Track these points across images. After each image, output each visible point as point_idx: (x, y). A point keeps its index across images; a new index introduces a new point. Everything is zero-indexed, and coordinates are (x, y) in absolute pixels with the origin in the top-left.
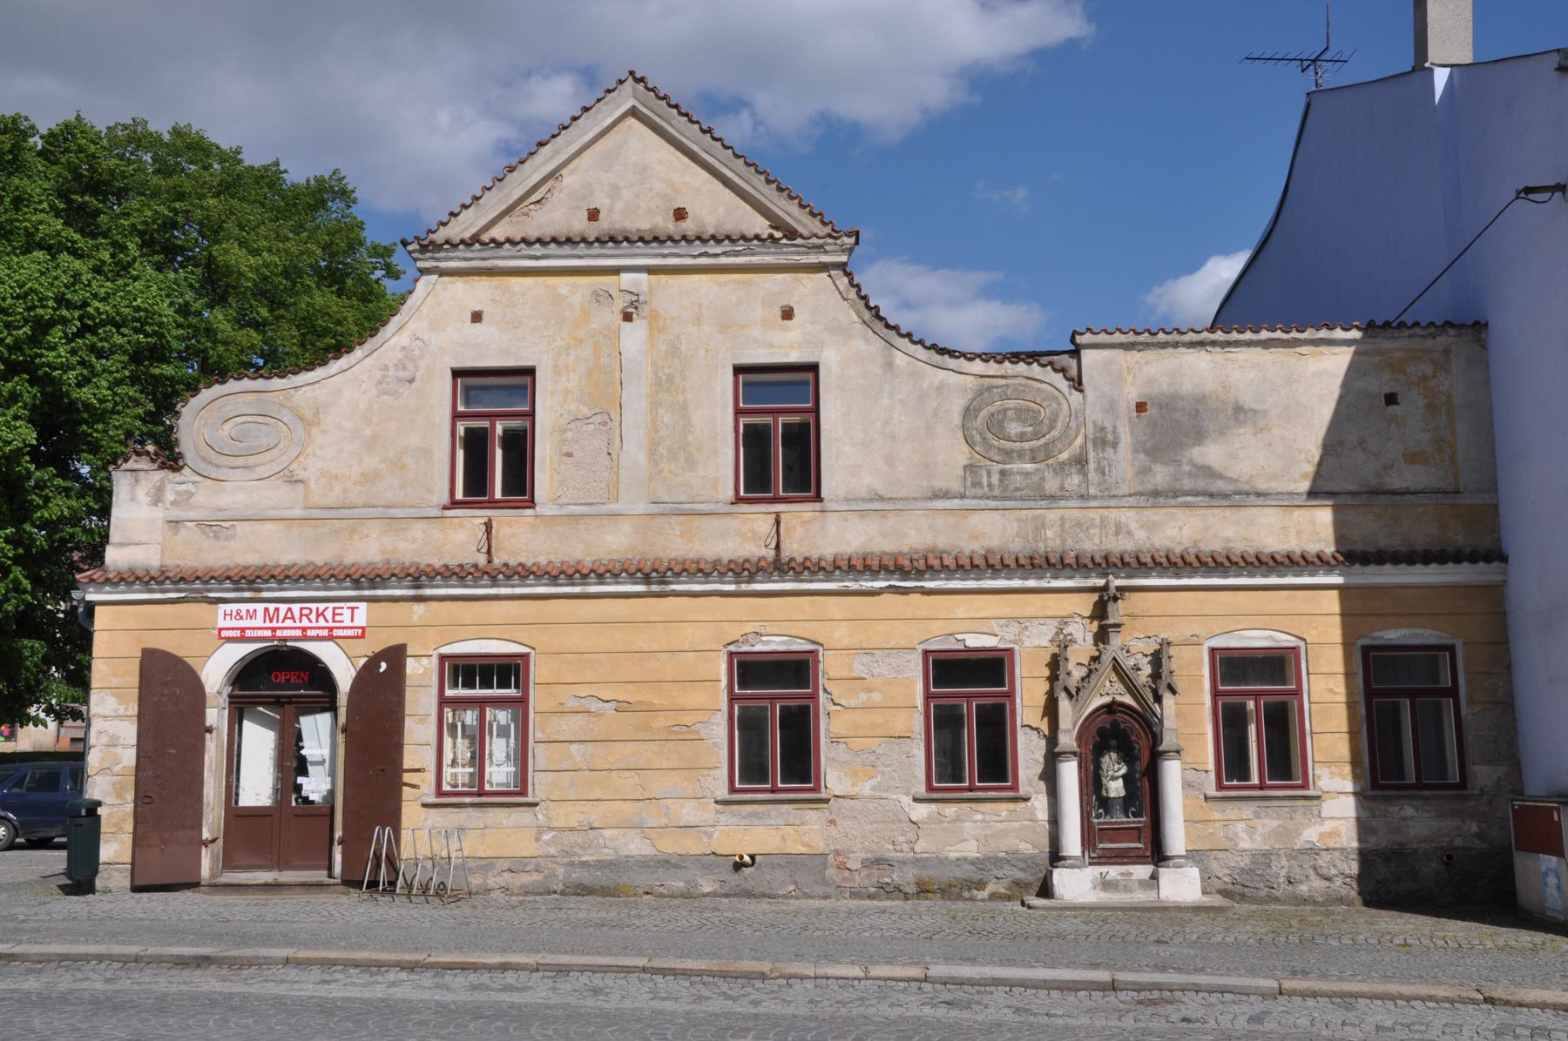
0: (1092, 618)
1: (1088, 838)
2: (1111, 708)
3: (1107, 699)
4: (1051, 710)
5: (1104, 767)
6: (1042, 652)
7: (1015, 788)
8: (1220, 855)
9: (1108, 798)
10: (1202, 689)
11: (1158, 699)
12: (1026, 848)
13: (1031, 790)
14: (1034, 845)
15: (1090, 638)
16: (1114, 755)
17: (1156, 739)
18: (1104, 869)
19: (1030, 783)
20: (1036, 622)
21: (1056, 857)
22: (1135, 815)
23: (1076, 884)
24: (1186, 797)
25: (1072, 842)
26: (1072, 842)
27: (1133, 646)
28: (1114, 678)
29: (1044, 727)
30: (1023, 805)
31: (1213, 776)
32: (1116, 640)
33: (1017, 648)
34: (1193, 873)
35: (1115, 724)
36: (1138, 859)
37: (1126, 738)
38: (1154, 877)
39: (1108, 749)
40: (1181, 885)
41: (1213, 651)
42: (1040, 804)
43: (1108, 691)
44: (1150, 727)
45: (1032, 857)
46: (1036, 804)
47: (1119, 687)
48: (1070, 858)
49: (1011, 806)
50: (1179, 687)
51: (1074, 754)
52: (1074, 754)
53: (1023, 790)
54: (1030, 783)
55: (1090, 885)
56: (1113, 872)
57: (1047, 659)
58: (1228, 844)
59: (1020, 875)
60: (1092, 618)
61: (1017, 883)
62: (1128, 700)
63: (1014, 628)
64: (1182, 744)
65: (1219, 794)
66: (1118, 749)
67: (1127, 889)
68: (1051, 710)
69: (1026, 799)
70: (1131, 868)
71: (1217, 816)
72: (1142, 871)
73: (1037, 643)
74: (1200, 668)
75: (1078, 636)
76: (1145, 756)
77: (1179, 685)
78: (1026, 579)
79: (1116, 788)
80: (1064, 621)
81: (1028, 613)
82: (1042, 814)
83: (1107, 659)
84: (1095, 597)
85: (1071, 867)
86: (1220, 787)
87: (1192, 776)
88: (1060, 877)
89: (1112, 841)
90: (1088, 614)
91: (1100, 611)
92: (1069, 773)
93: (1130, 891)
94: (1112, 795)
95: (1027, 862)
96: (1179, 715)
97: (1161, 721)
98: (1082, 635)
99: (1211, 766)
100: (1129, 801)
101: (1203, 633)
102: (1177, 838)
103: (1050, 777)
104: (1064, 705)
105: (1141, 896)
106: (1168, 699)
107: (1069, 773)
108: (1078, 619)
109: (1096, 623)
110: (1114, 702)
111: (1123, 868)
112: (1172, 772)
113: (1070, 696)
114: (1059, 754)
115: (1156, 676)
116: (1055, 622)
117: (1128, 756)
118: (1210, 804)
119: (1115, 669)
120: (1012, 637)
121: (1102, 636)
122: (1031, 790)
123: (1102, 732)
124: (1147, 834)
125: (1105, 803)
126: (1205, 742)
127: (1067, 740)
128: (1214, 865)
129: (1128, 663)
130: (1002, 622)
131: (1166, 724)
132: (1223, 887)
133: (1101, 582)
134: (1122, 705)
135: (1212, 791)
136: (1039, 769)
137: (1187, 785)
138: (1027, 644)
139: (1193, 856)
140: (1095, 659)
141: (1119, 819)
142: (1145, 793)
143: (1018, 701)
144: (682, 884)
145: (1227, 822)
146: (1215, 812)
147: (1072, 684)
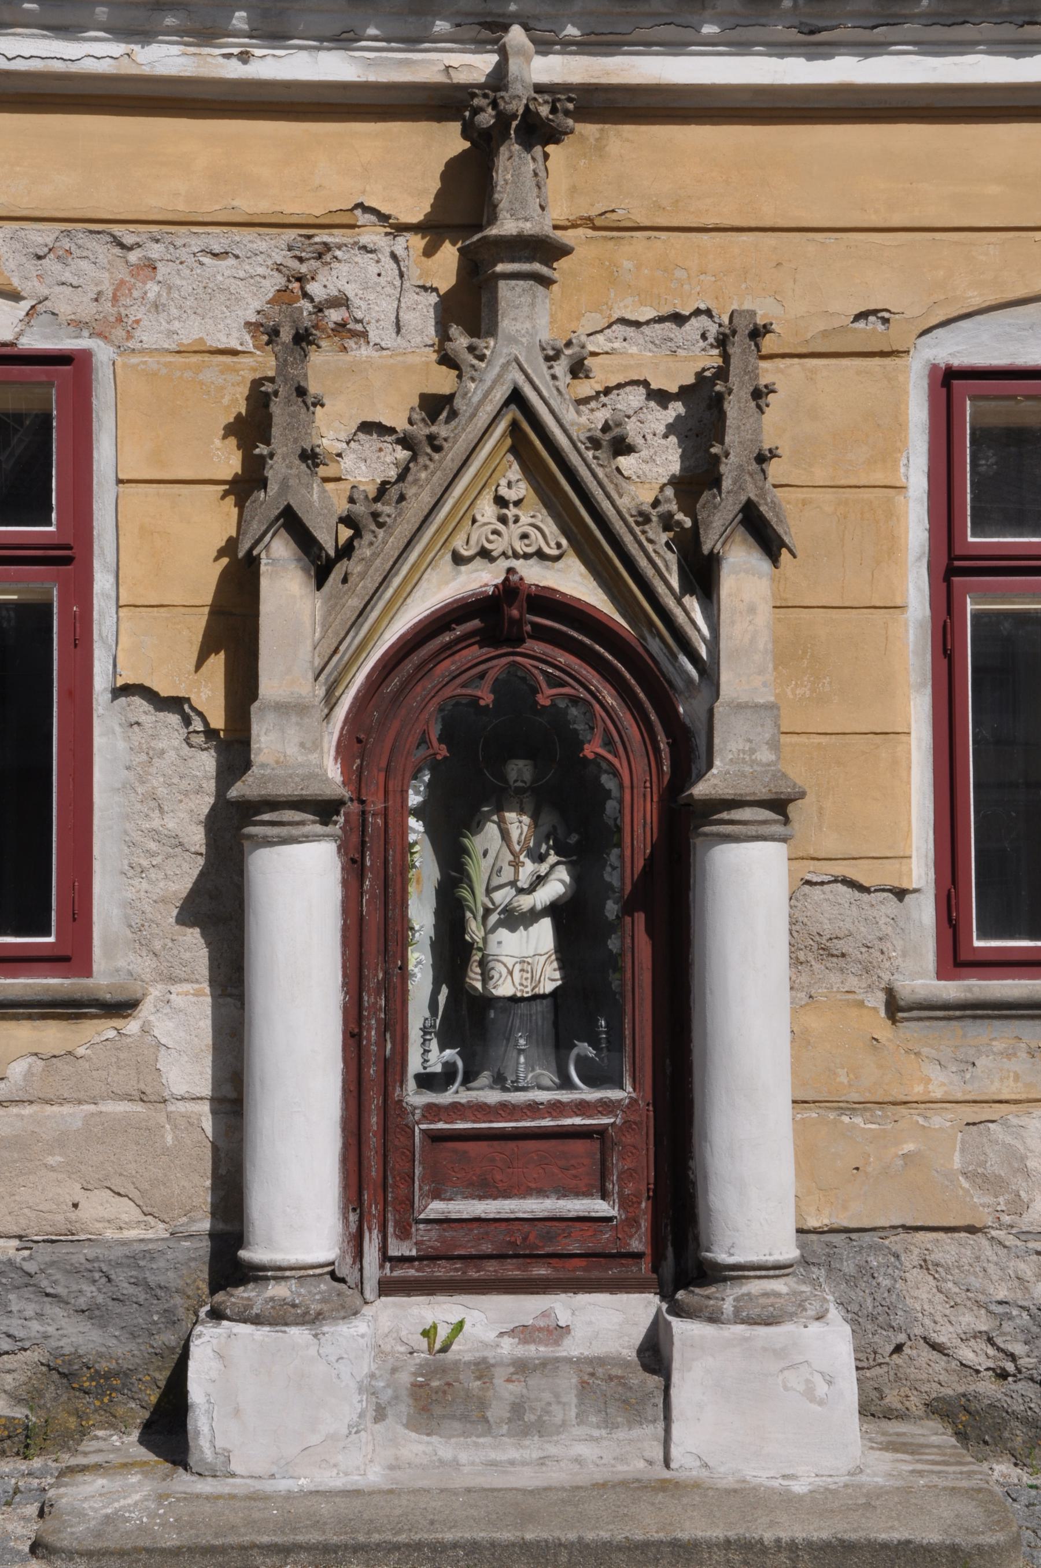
0: (433, 230)
1: (379, 1163)
2: (499, 616)
3: (482, 578)
4: (233, 626)
5: (479, 870)
6: (213, 370)
7: (73, 957)
8: (947, 1249)
9: (488, 1001)
10: (891, 546)
11: (702, 575)
12: (114, 1220)
13: (143, 965)
14: (139, 1211)
15: (421, 316)
16: (519, 824)
17: (686, 749)
18: (441, 1311)
19: (140, 936)
20: (196, 240)
21: (229, 1264)
22: (592, 1080)
23: (292, 1407)
24: (804, 999)
25: (301, 1209)
26: (301, 1209)
27: (610, 341)
28: (515, 483)
29: (209, 695)
30: (105, 1029)
31: (924, 911)
32: (528, 317)
33: (103, 353)
34: (829, 1344)
35: (516, 690)
36: (591, 1265)
37: (557, 740)
38: (655, 1354)
39: (501, 798)
40: (773, 1410)
41: (948, 380)
42: (178, 1025)
43: (496, 540)
44: (665, 693)
45: (137, 1258)
46: (164, 1029)
47: (538, 525)
48: (279, 1272)
49: (52, 1035)
50: (795, 523)
51: (324, 810)
52: (324, 810)
53: (109, 967)
54: (140, 936)
55: (351, 1406)
56: (483, 1323)
57: (235, 402)
58: (980, 1205)
59: (78, 1337)
60: (433, 230)
61: (66, 1372)
62: (574, 581)
63: (96, 266)
64: (798, 774)
65: (953, 990)
66: (539, 801)
67: (524, 1421)
68: (233, 626)
69: (121, 1008)
70: (561, 1306)
71: (939, 1082)
72: (608, 1321)
73: (191, 331)
74: (890, 452)
75: (374, 307)
76: (638, 821)
77: (795, 518)
78: (144, 35)
79: (523, 960)
80: (314, 239)
81: (153, 205)
82: (188, 1073)
83: (483, 395)
84: (449, 141)
85: (277, 1317)
86: (955, 959)
87: (835, 909)
88: (224, 1364)
89: (486, 1190)
90: (415, 208)
91: (464, 204)
92: (300, 886)
93: (540, 1428)
94: (504, 988)
95: (112, 1281)
96: (790, 654)
97: (709, 672)
98: (393, 292)
99: (920, 871)
100: (575, 1011)
101: (907, 302)
102: (758, 1190)
103: (220, 908)
104: (285, 592)
105: (586, 1453)
106: (742, 573)
107: (300, 886)
108: (373, 236)
109: (449, 254)
110: (510, 590)
111: (528, 1307)
112: (748, 886)
113: (321, 567)
114: (249, 810)
115: (698, 480)
116: (274, 247)
117: (576, 824)
118: (912, 1031)
119: (519, 447)
120: (87, 310)
121: (468, 308)
122: (143, 965)
123: (460, 724)
124: (635, 1161)
125: (472, 1020)
126: (899, 766)
127: (299, 749)
128: (921, 1294)
129: (571, 421)
130: (41, 236)
131: (733, 683)
132: (954, 1387)
133: (475, 66)
134: (548, 603)
135: (920, 977)
136: (183, 875)
137: (814, 950)
138: (151, 334)
139: (827, 1249)
140: (435, 406)
141: (534, 1086)
142: (639, 980)
143: (102, 582)
144: (368, 864)
145: (981, 1111)
146: (932, 1067)
147: (323, 507)
